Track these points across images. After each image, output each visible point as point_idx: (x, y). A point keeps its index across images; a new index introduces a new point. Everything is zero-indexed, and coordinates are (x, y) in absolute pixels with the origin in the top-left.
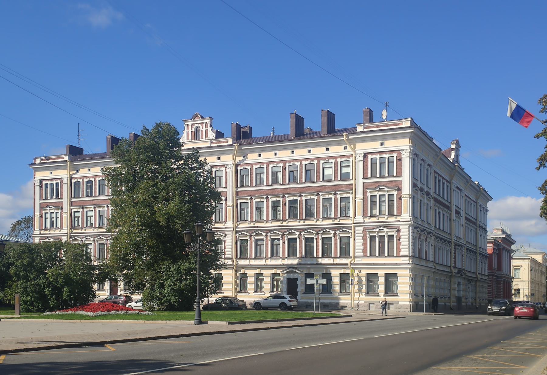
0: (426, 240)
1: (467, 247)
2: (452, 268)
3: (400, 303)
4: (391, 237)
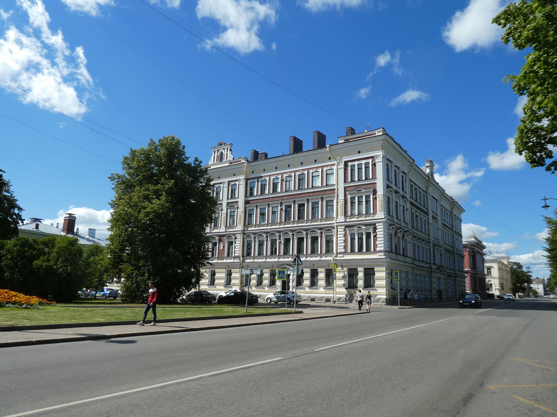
0: (403, 238)
1: (445, 248)
2: (432, 264)
3: (378, 296)
4: (368, 235)
